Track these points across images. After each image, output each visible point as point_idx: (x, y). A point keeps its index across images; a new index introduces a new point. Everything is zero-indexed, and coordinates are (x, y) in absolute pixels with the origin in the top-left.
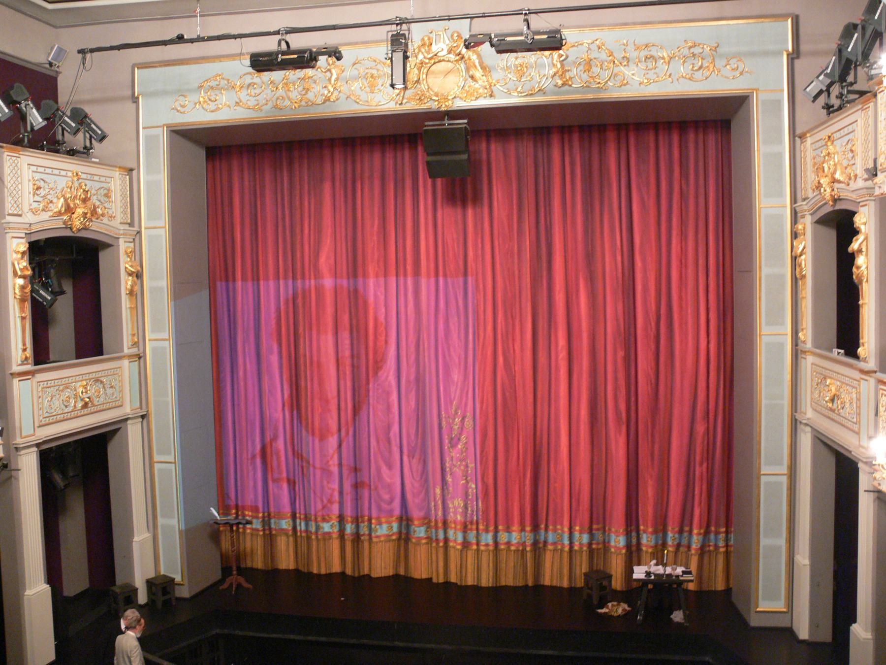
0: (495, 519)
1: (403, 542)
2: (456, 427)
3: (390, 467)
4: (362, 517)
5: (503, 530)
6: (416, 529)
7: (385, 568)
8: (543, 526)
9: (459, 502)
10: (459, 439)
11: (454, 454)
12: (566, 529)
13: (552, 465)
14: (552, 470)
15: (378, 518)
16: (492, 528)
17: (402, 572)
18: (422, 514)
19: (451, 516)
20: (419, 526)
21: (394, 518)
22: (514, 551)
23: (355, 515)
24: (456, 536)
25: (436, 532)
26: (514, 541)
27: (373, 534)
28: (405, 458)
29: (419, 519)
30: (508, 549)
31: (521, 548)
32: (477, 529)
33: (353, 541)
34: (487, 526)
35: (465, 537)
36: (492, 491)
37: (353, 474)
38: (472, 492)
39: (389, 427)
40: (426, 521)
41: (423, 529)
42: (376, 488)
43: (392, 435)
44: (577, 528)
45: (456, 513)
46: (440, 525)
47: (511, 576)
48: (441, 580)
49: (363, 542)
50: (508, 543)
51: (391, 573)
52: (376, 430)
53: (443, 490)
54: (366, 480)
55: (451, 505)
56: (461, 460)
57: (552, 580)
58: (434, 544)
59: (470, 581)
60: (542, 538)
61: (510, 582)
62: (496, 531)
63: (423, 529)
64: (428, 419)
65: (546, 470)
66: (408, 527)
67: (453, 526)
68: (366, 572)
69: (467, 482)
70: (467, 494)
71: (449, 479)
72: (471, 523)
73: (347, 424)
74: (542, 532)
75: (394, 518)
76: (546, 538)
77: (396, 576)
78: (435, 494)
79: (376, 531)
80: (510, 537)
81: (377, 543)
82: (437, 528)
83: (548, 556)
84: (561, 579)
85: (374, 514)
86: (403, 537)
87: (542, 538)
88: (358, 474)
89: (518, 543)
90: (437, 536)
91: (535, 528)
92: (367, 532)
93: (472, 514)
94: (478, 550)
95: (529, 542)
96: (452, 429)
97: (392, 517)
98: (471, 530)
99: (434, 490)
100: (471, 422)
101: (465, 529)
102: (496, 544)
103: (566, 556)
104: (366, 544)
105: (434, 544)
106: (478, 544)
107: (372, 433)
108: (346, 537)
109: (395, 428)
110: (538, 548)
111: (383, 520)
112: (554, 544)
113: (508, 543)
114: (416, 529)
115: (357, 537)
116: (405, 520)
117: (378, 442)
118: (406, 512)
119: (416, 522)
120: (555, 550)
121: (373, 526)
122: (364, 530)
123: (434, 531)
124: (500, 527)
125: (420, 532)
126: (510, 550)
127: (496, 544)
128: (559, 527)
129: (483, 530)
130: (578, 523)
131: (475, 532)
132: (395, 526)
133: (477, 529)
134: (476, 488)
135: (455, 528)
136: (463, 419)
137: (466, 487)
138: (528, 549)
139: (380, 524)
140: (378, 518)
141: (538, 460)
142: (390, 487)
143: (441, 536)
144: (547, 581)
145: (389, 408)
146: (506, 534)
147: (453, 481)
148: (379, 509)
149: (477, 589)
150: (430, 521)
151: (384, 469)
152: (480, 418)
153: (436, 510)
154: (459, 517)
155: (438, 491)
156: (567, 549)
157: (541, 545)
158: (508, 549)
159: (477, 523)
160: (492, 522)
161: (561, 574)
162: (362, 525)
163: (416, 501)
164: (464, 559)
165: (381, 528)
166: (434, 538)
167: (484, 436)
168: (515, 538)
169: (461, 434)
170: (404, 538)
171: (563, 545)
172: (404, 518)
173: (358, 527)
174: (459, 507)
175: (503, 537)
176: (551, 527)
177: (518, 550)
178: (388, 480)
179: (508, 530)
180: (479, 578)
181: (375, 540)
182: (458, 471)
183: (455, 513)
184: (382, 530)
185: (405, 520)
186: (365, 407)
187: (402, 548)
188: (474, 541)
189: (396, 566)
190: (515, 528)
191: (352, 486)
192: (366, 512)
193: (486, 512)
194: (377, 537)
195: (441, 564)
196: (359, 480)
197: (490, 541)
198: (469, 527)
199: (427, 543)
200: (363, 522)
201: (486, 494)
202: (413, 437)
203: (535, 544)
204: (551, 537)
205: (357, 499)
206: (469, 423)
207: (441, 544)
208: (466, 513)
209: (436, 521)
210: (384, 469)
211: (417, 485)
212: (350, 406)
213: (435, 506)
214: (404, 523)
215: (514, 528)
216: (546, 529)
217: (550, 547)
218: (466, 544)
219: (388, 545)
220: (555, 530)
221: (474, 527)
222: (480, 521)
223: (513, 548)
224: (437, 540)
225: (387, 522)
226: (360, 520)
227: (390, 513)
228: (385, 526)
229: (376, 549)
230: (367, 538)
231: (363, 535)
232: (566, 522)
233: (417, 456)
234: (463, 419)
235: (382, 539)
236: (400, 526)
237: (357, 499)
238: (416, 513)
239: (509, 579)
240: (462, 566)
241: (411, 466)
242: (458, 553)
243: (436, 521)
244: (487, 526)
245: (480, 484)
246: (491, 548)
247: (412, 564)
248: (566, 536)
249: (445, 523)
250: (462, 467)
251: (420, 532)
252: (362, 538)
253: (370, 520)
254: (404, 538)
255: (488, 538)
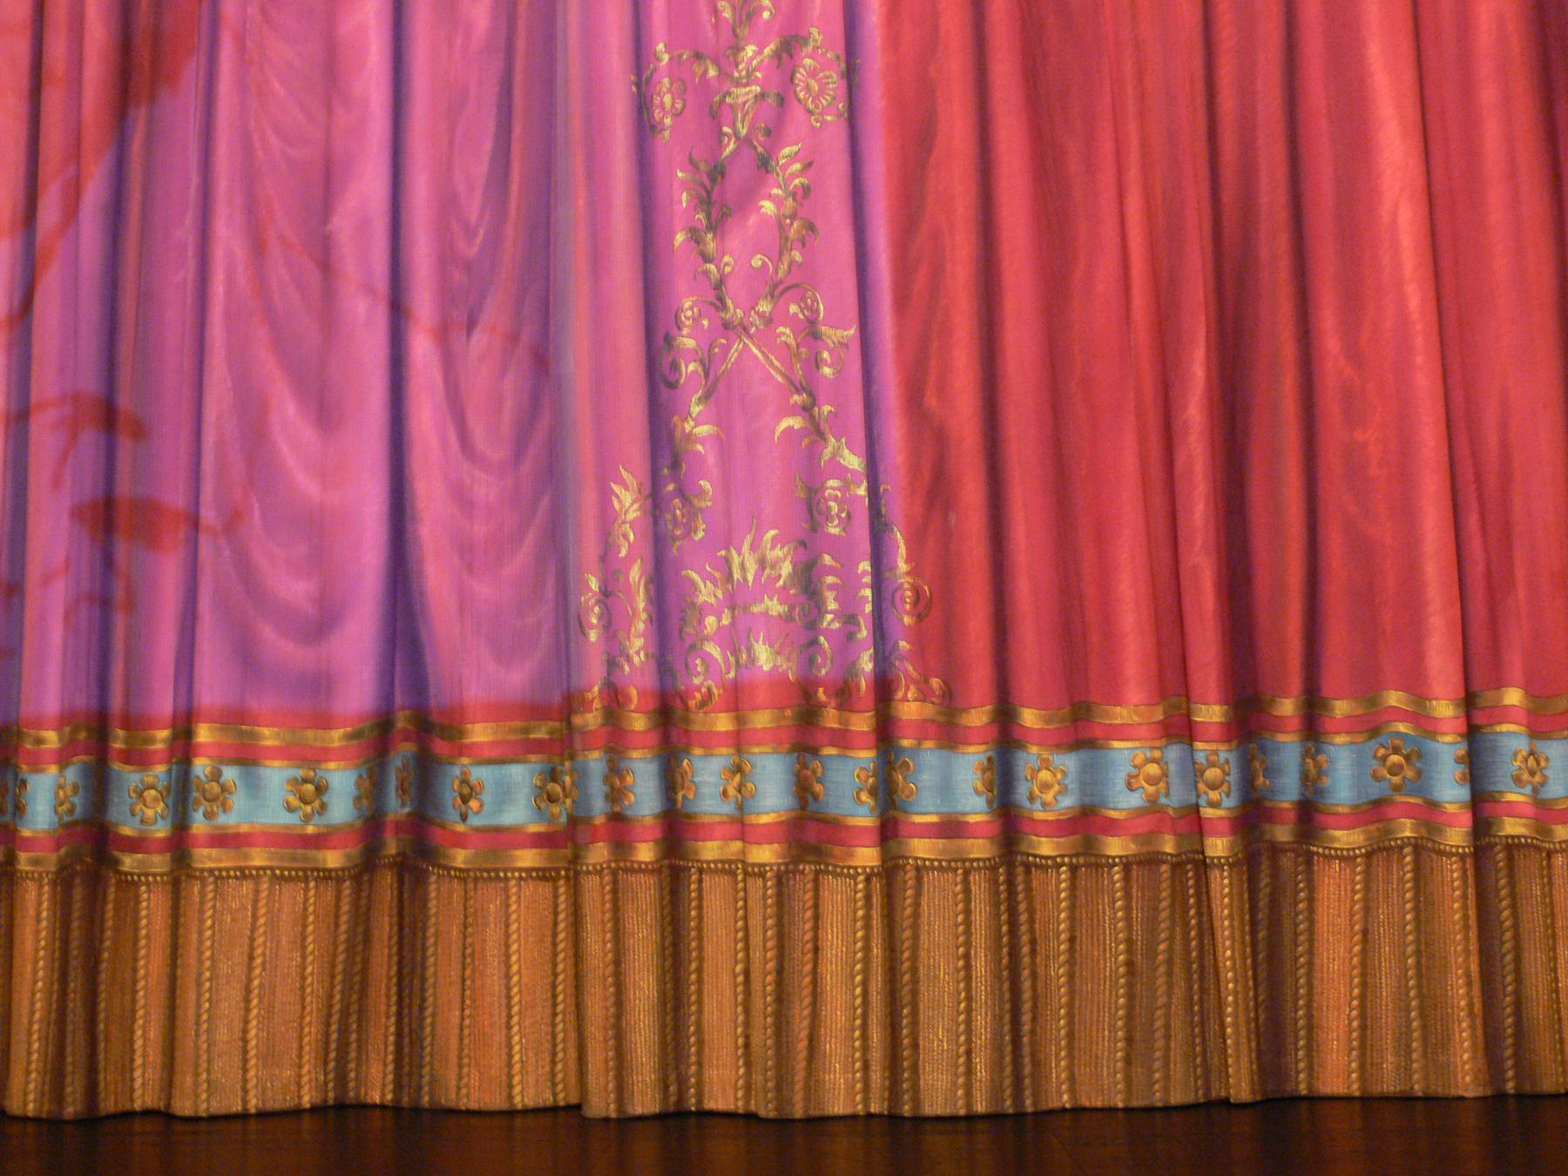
0: (1009, 655)
1: (387, 879)
2: (744, 95)
3: (326, 412)
4: (136, 723)
5: (1044, 739)
6: (479, 774)
7: (269, 1056)
8: (1287, 707)
9: (761, 558)
10: (764, 165)
11: (737, 256)
12: (1445, 709)
13: (1328, 320)
14: (1331, 342)
15: (235, 717)
16: (978, 717)
17: (377, 1087)
18: (517, 679)
19: (707, 670)
20: (502, 756)
21: (336, 737)
22: (1127, 865)
23: (83, 701)
24: (742, 788)
25: (615, 770)
26: (1124, 801)
27: (199, 824)
28: (422, 347)
29: (497, 711)
30: (1087, 861)
31: (1168, 846)
32: (885, 733)
33: (63, 879)
34: (951, 702)
35: (803, 789)
36: (978, 486)
37: (90, 438)
38: (847, 501)
39: (327, 181)
40: (552, 728)
41: (522, 776)
42: (233, 520)
43: (342, 225)
44: (1513, 697)
45: (745, 628)
46: (639, 723)
47: (1109, 1045)
48: (645, 1101)
49: (129, 885)
50: (1087, 822)
51: (307, 1088)
52: (249, 178)
53: (655, 502)
54: (175, 496)
55: (707, 593)
56: (779, 291)
57: (1366, 1067)
58: (599, 853)
59: (843, 1089)
60: (1288, 790)
61: (1107, 1086)
62: (1006, 738)
63: (522, 776)
64: (572, 66)
65: (1289, 352)
66: (425, 772)
67: (723, 723)
68: (144, 1094)
69: (816, 431)
70: (813, 509)
71: (697, 425)
72: (844, 694)
73: (75, 152)
74: (1288, 748)
75: (336, 737)
76: (1312, 782)
77: (340, 1113)
78: (607, 517)
79: (221, 799)
80: (1092, 778)
81: (220, 877)
82: (616, 740)
83: (1335, 897)
84: (1436, 1042)
85: (212, 690)
86: (391, 847)
87: (1288, 790)
88: (125, 446)
89: (1153, 808)
90: (615, 795)
91: (1248, 724)
92: (161, 831)
93: (847, 637)
94: (890, 870)
95: (1219, 806)
96: (714, 115)
97: (324, 721)
98: (843, 740)
99: (605, 496)
100: (834, 80)
101: (805, 738)
102: (1009, 822)
103: (1452, 878)
104: (152, 907)
105: (599, 853)
106: (889, 830)
107: (223, 184)
108: (24, 860)
109: (368, 187)
110: (1281, 847)
111: (269, 736)
112: (1374, 811)
113: (1087, 822)
114: (479, 774)
115: (93, 843)
116: (411, 735)
117: (258, 247)
118: (418, 683)
119: (480, 733)
120: (1380, 851)
121: (201, 767)
122: (141, 807)
123: (595, 762)
124: (1029, 717)
125: (505, 795)
126: (1099, 864)
127: (1009, 822)
128: (1394, 698)
129: (923, 730)
130: (1515, 662)
131: (866, 756)
132: (342, 781)
133: (885, 733)
134: (873, 474)
135: (739, 740)
136: (789, 49)
137: (812, 473)
138: (1218, 846)
139: (247, 757)
140: (235, 717)
141: (1250, 287)
142: (317, 532)
143: (644, 799)
144: (1337, 1073)
145: (332, 71)
146: (1069, 762)
147: (723, 444)
148: (246, 656)
149: (898, 1131)
150: (571, 704)
151: (288, 416)
152: (893, 40)
153: (611, 627)
154: (764, 657)
155: (628, 502)
156: (1456, 837)
157: (1283, 833)
158: (1087, 861)
159: (884, 688)
160: (980, 675)
161: (1431, 1005)
162: (129, 777)
163: (483, 590)
164: (802, 931)
165: (254, 787)
166: (599, 808)
167: (917, 143)
168: (1133, 772)
169: (775, 134)
170: (400, 855)
171: (1430, 812)
172: (402, 721)
173: (99, 785)
174: (766, 587)
175: (1050, 782)
176: (1341, 708)
177: (1151, 860)
178: (307, 485)
179: (1081, 733)
180: (899, 1056)
181: (206, 858)
182: (760, 361)
183: (734, 640)
184: (262, 801)
185: (411, 735)
186: (190, 76)
187: (384, 925)
188: (863, 816)
189: (340, 1050)
190: (1131, 710)
191: (77, 514)
192: (164, 703)
193: (938, 607)
194: (223, 840)
195: (644, 987)
196: (123, 488)
197: (975, 806)
198: (831, 718)
199: (543, 875)
200: (137, 757)
201: (936, 492)
202: (474, 206)
203: (1252, 815)
204: (1346, 773)
205: (104, 603)
206: (818, 81)
207: (645, 853)
208: (812, 625)
209: (614, 698)
210: (288, 416)
211: (486, 489)
212: (96, 70)
213: (606, 593)
214: (402, 753)
215: (1122, 715)
216: (1313, 727)
217: (1345, 838)
218: (810, 835)
219: (291, 895)
220: (1371, 726)
221: (862, 723)
222: (906, 669)
223: (1115, 847)
224: (620, 827)
225: (287, 753)
226: (119, 740)
227: (313, 697)
228: (277, 776)
229: (220, 918)
230: (159, 863)
231: (136, 845)
232: (1441, 662)
233: (495, 312)
234: (789, 49)
235: (258, 858)
236: (372, 790)
237: (104, 603)
238: (479, 672)
239: (1090, 1070)
240: (786, 988)
241: (460, 393)
242: (761, 893)
243: (614, 698)
244: (951, 702)
245: (894, 432)
246: (980, 849)
247: (445, 1014)
248: (1447, 750)
249: (670, 715)
250: (786, 333)
251: (502, 795)
252: (129, 862)
253: (183, 748)
254: (400, 855)
255: (950, 783)
